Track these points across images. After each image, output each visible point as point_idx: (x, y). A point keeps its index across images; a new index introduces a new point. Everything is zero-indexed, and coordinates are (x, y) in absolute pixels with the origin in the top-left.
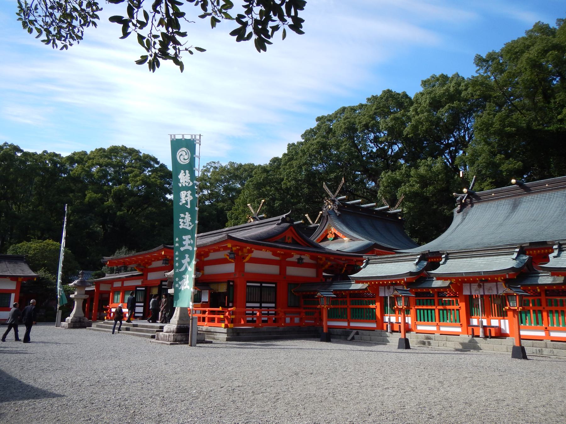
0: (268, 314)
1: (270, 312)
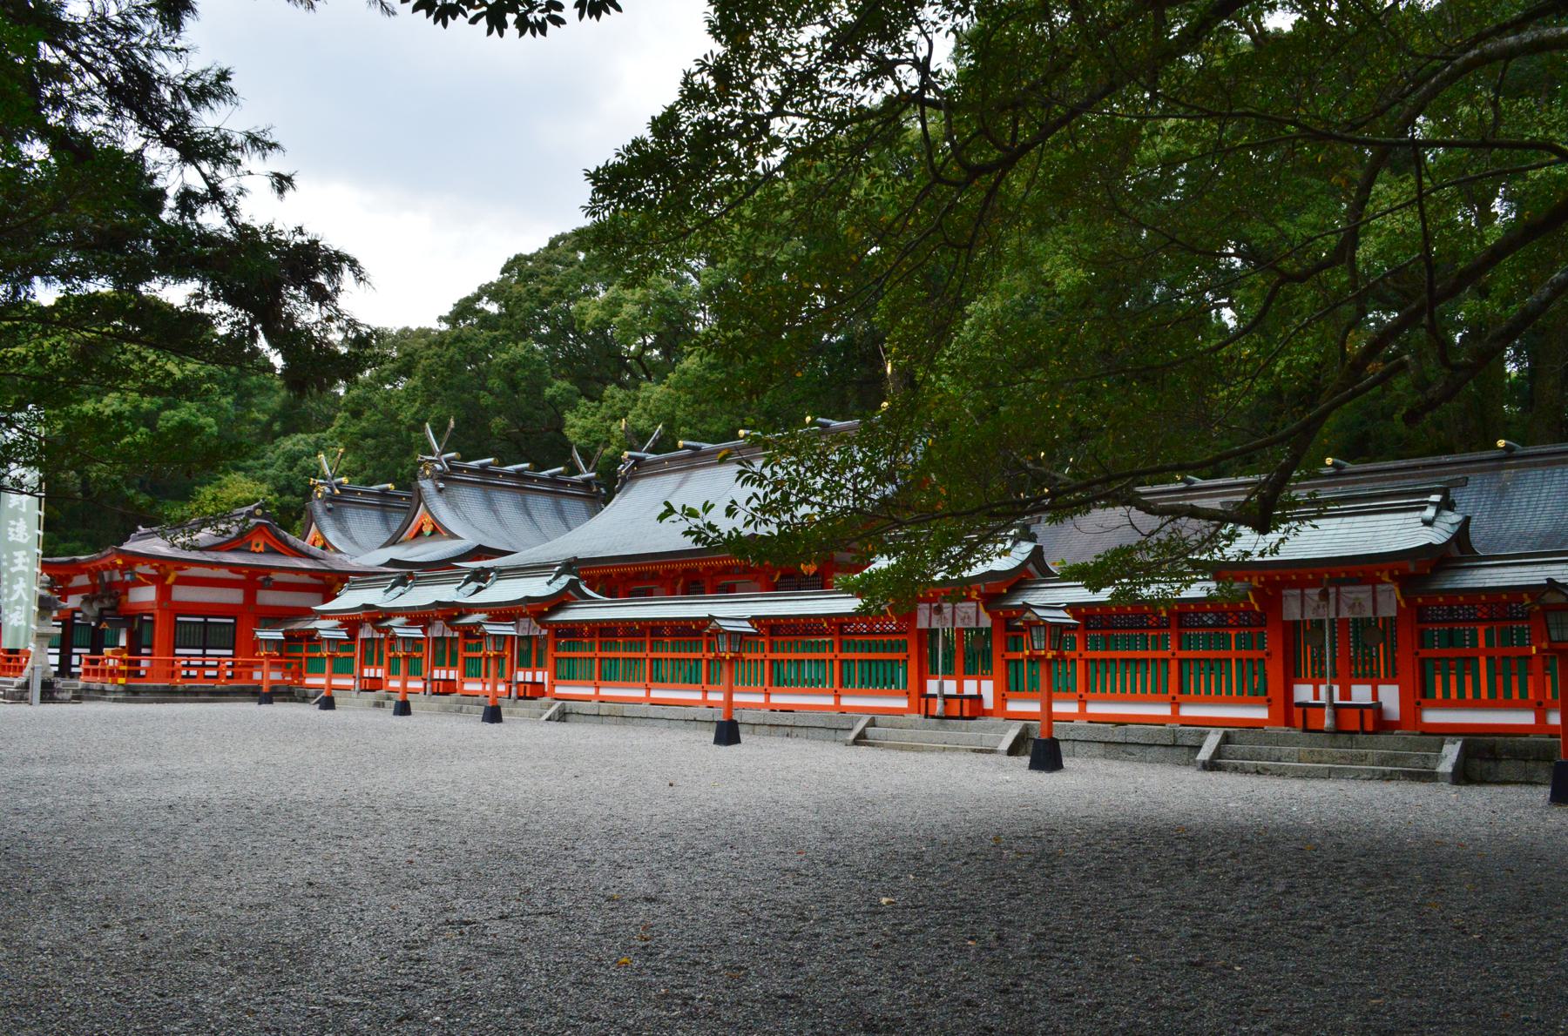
0: (188, 666)
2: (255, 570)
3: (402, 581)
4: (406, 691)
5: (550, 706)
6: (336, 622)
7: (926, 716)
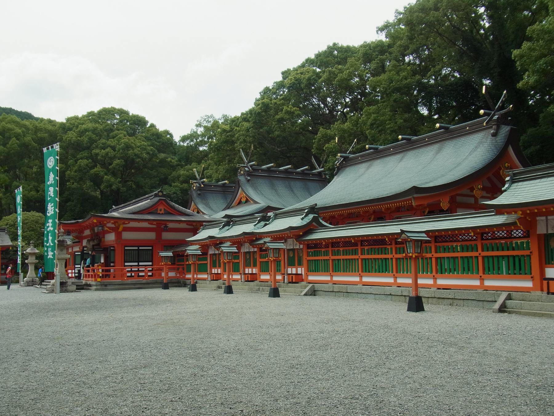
0: (131, 271)
1: (140, 269)
2: (159, 222)
3: (227, 224)
5: (305, 287)
6: (197, 247)
7: (548, 293)
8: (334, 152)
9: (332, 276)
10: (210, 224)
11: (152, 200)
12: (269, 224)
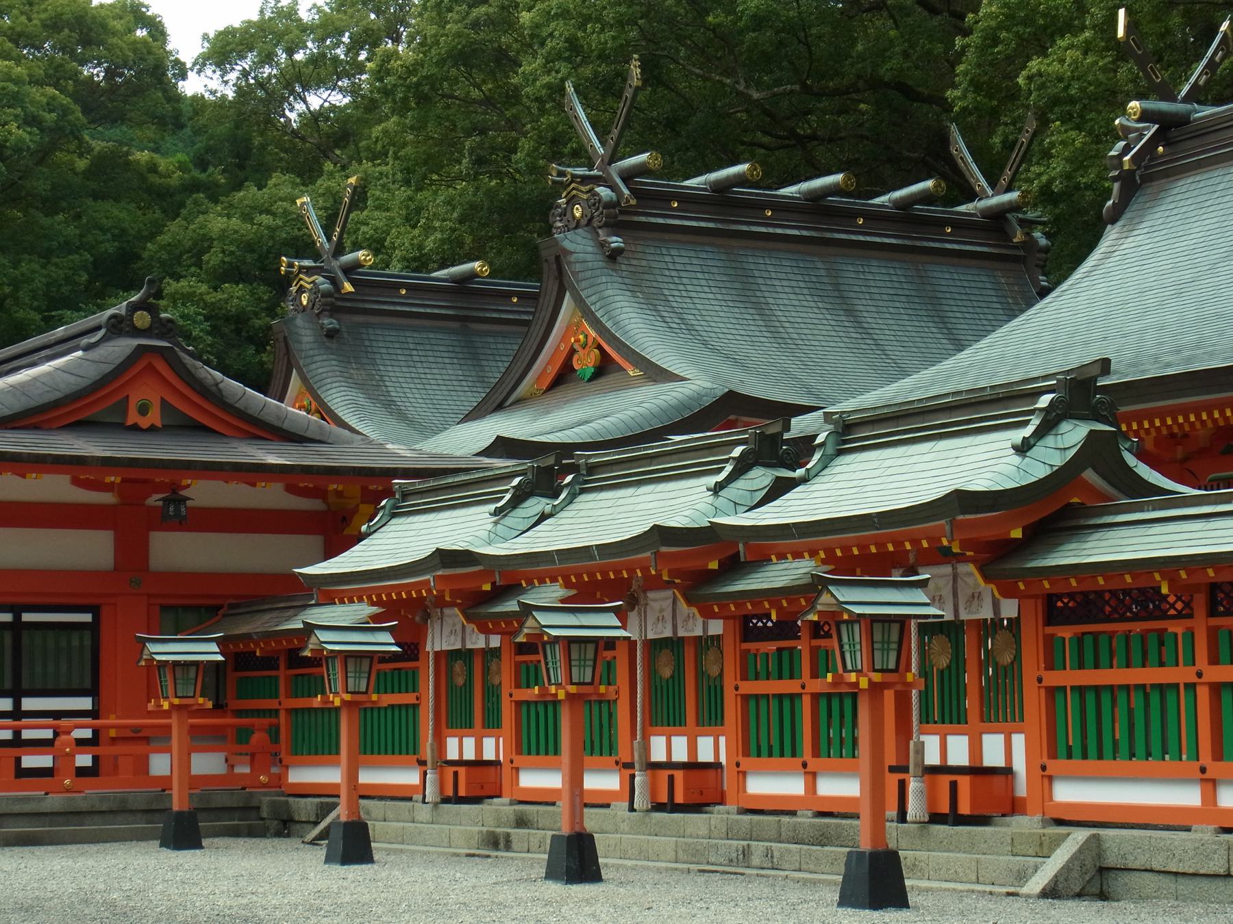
1: (27, 734)
2: (137, 475)
4: (582, 801)
5: (1044, 850)
6: (362, 611)
8: (1072, 101)
9: (812, 778)
10: (432, 483)
11: (93, 355)
12: (804, 480)
